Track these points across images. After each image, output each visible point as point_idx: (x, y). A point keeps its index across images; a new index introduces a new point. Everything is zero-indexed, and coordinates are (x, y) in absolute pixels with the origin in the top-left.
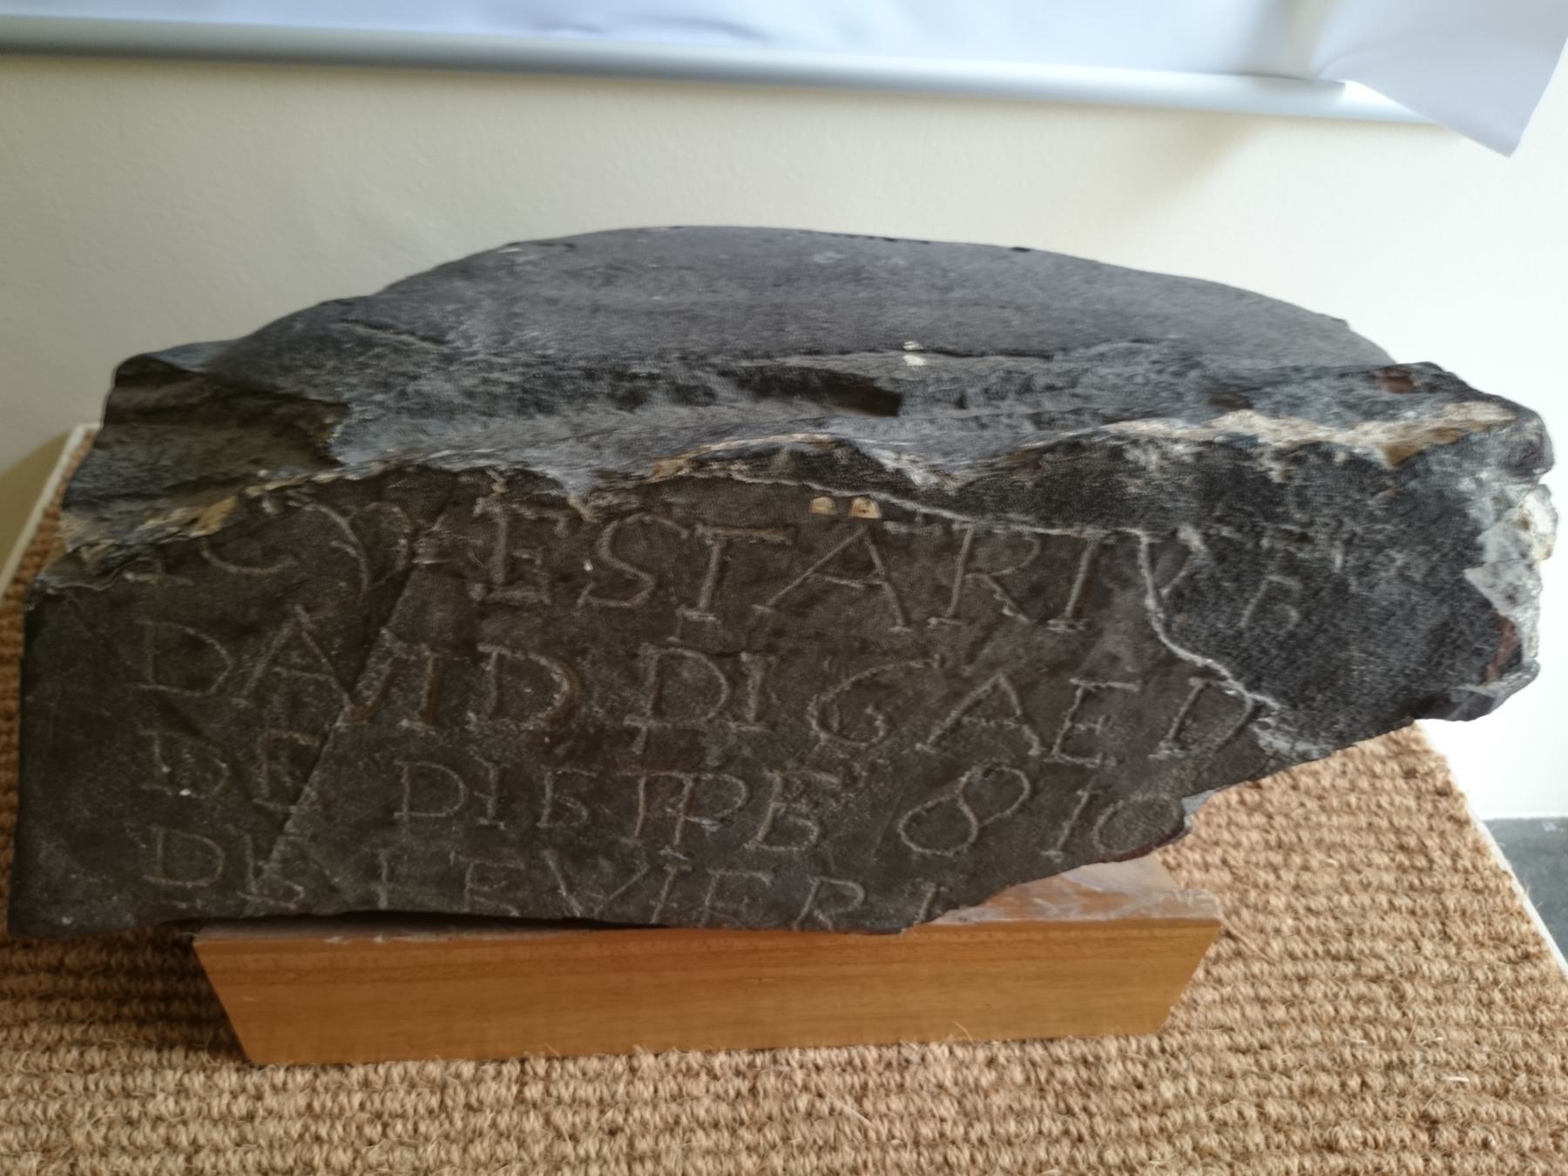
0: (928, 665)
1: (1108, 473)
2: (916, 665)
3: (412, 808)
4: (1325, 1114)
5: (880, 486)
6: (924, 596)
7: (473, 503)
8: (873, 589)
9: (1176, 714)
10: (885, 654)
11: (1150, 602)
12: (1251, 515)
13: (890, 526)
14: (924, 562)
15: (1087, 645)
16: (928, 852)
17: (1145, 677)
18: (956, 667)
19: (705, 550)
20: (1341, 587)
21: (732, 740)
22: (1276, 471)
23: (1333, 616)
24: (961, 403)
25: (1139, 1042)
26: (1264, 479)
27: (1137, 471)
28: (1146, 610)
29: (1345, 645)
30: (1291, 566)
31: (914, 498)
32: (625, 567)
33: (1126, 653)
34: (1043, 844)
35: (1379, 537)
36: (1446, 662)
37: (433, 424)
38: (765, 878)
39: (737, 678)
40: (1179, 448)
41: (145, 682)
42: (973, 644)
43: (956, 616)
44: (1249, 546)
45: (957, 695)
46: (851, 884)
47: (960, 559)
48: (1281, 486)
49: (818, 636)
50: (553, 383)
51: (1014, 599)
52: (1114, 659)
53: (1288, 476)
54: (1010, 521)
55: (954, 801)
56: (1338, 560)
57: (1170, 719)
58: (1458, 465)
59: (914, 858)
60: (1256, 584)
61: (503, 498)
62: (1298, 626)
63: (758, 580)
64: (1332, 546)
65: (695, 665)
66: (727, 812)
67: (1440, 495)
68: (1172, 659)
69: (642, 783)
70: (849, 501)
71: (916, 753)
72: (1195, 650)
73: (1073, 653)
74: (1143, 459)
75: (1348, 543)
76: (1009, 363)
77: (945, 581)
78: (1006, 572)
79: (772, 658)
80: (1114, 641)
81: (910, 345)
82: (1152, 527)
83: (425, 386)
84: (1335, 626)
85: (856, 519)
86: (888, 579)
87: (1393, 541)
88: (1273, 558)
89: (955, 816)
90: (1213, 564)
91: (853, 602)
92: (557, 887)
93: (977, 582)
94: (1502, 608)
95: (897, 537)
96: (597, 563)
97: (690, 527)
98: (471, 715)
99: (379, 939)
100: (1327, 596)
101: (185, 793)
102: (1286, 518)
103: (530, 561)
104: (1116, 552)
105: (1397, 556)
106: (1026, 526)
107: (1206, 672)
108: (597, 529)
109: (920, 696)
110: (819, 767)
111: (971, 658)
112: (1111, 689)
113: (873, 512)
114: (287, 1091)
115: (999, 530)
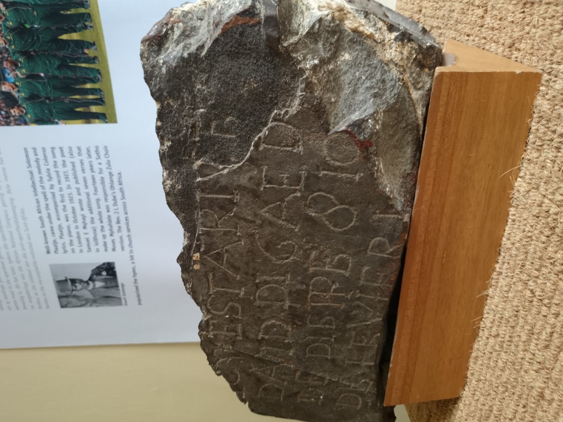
0: (257, 233)
1: (175, 195)
2: (257, 236)
3: (327, 355)
4: (559, 24)
5: (189, 254)
6: (228, 238)
7: (210, 338)
8: (227, 251)
9: (279, 150)
10: (253, 246)
11: (226, 171)
12: (186, 148)
13: (202, 249)
14: (215, 239)
15: (245, 188)
16: (354, 220)
17: (259, 166)
18: (257, 226)
19: (217, 292)
20: (213, 107)
21: (294, 282)
23: (227, 105)
25: (542, 85)
26: (170, 148)
27: (173, 187)
28: (228, 172)
29: (241, 96)
30: (207, 126)
31: (192, 244)
32: (226, 309)
33: (248, 175)
35: (189, 98)
36: (249, 46)
38: (366, 268)
39: (266, 282)
40: (165, 174)
41: (280, 399)
42: (247, 222)
43: (236, 228)
44: (199, 144)
46: (372, 242)
47: (213, 230)
48: (172, 141)
49: (247, 264)
51: (227, 213)
53: (169, 140)
54: (197, 218)
55: (325, 216)
56: (202, 110)
57: (282, 151)
58: (156, 77)
59: (357, 224)
60: (215, 137)
61: (208, 331)
62: (233, 116)
63: (227, 280)
64: (196, 115)
65: (263, 291)
66: (329, 281)
67: (168, 81)
69: (313, 304)
70: (194, 261)
71: (300, 231)
72: (248, 150)
73: (248, 192)
74: (169, 186)
75: (194, 109)
77: (222, 233)
78: (216, 217)
79: (258, 274)
80: (244, 180)
82: (195, 177)
84: (231, 103)
85: (200, 258)
86: (223, 248)
87: (191, 92)
88: (203, 135)
90: (208, 154)
91: (232, 256)
92: (366, 325)
93: (221, 224)
95: (206, 248)
96: (226, 314)
97: (210, 295)
98: (286, 341)
99: (391, 366)
100: (218, 109)
101: (321, 397)
102: (185, 136)
103: (227, 328)
104: (203, 187)
105: (198, 87)
107: (257, 146)
109: (272, 234)
111: (253, 222)
112: (265, 176)
113: (198, 255)
114: (466, 393)
115: (200, 221)
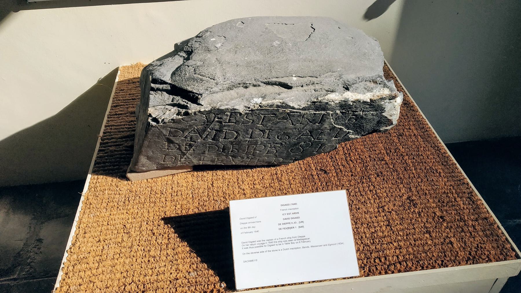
22: (351, 104)
24: (302, 86)
27: (330, 105)
34: (313, 151)
37: (214, 95)
45: (300, 134)
50: (233, 86)
52: (326, 128)
68: (335, 127)
76: (310, 79)
81: (294, 75)
83: (213, 89)
89: (299, 148)
94: (389, 118)
106: (313, 112)
108: (244, 115)
110: (277, 144)
111: (303, 129)
